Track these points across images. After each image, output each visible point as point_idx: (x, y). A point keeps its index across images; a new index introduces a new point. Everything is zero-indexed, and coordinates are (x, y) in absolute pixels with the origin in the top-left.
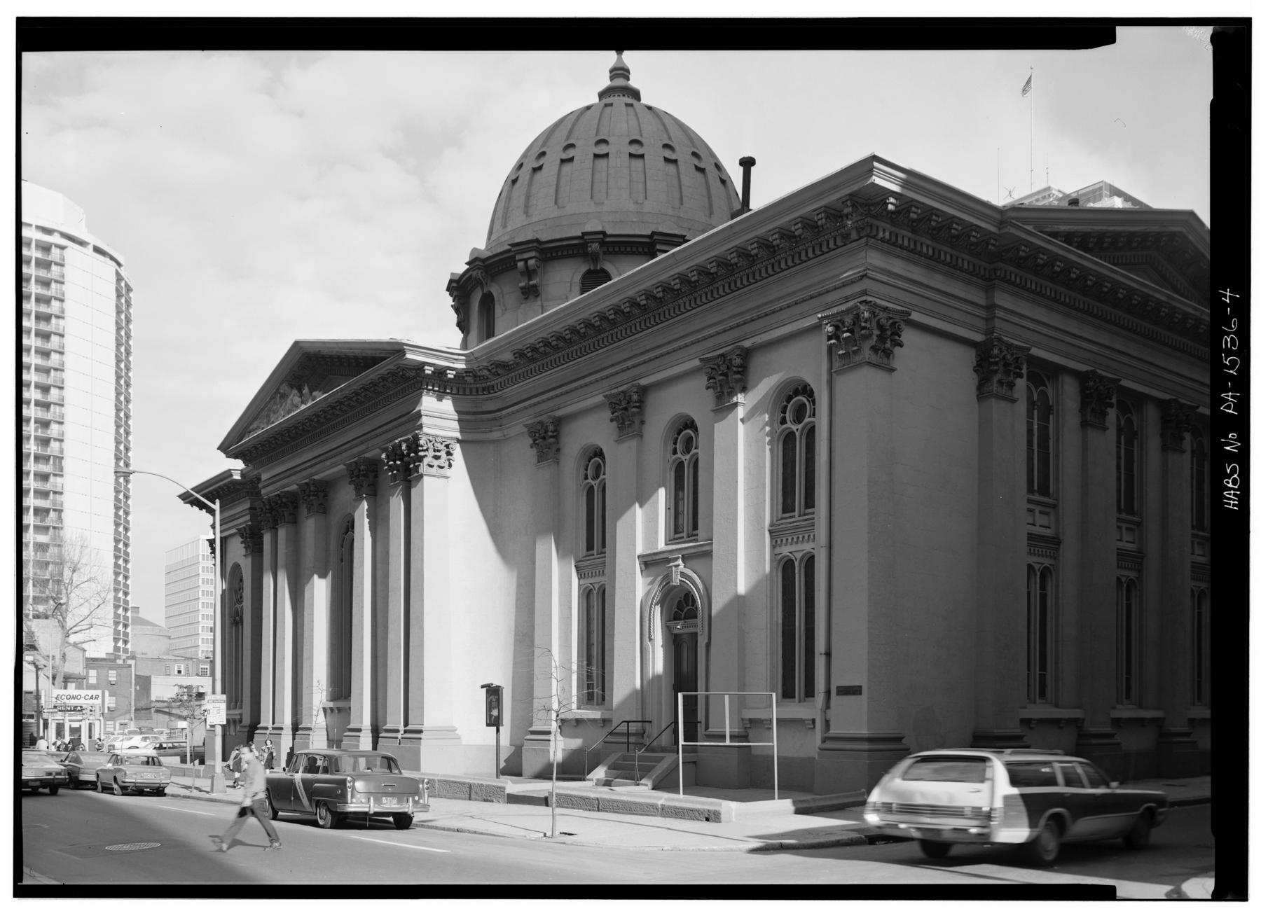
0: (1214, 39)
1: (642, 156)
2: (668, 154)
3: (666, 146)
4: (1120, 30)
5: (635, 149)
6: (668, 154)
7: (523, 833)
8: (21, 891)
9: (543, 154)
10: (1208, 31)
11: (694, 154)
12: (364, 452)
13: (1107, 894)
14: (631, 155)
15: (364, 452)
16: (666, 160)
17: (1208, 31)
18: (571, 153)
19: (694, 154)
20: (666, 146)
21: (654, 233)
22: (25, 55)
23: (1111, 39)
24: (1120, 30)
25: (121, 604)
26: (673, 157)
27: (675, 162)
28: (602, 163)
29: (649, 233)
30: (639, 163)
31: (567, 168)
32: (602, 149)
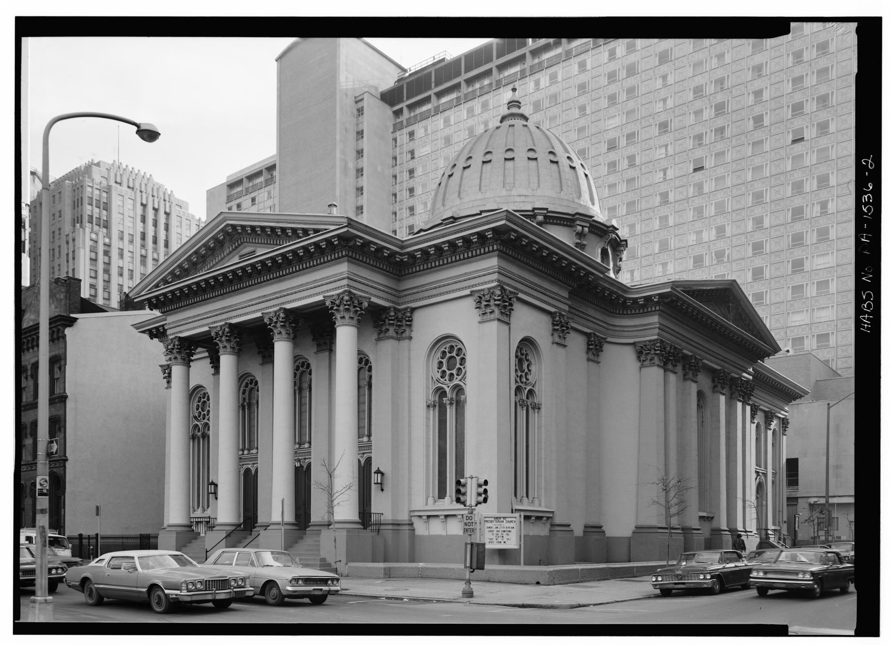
0: (858, 31)
1: (536, 159)
2: (552, 157)
3: (551, 152)
4: (793, 24)
5: (531, 155)
6: (552, 157)
7: (120, 541)
8: (20, 628)
9: (470, 157)
10: (854, 25)
11: (568, 158)
12: (230, 318)
13: (781, 631)
14: (529, 158)
15: (230, 318)
16: (552, 162)
17: (854, 25)
18: (488, 157)
19: (568, 158)
20: (551, 152)
21: (534, 209)
22: (24, 40)
23: (787, 31)
24: (793, 24)
25: (331, 495)
26: (555, 160)
27: (557, 162)
28: (509, 164)
29: (531, 209)
30: (533, 163)
31: (488, 167)
32: (509, 155)
